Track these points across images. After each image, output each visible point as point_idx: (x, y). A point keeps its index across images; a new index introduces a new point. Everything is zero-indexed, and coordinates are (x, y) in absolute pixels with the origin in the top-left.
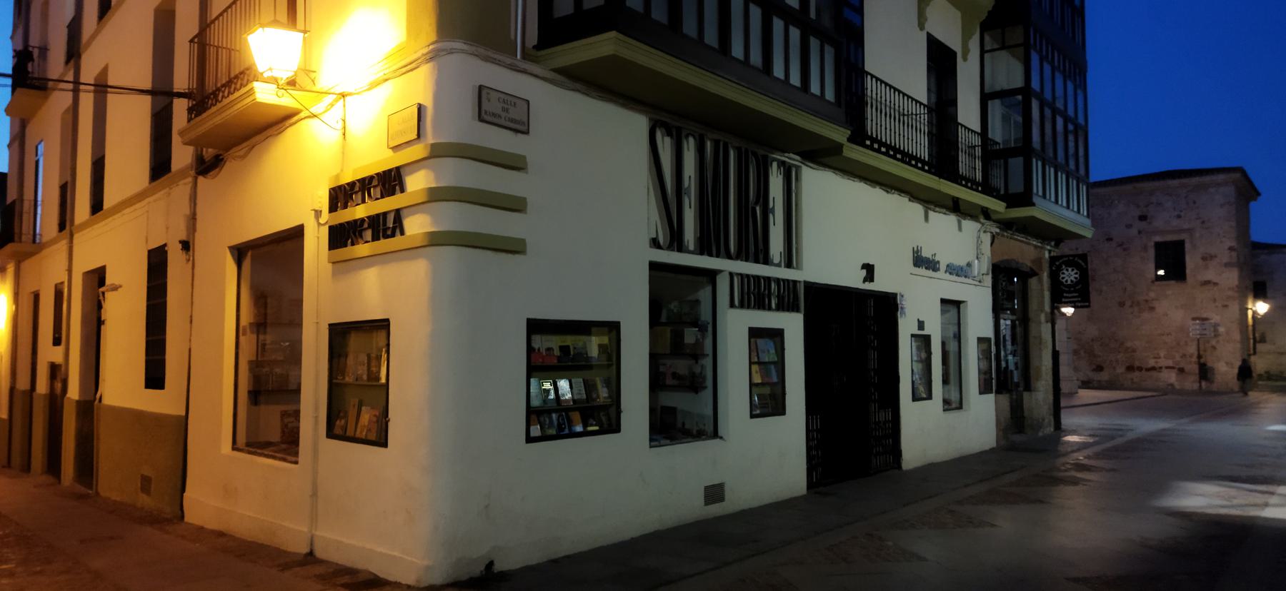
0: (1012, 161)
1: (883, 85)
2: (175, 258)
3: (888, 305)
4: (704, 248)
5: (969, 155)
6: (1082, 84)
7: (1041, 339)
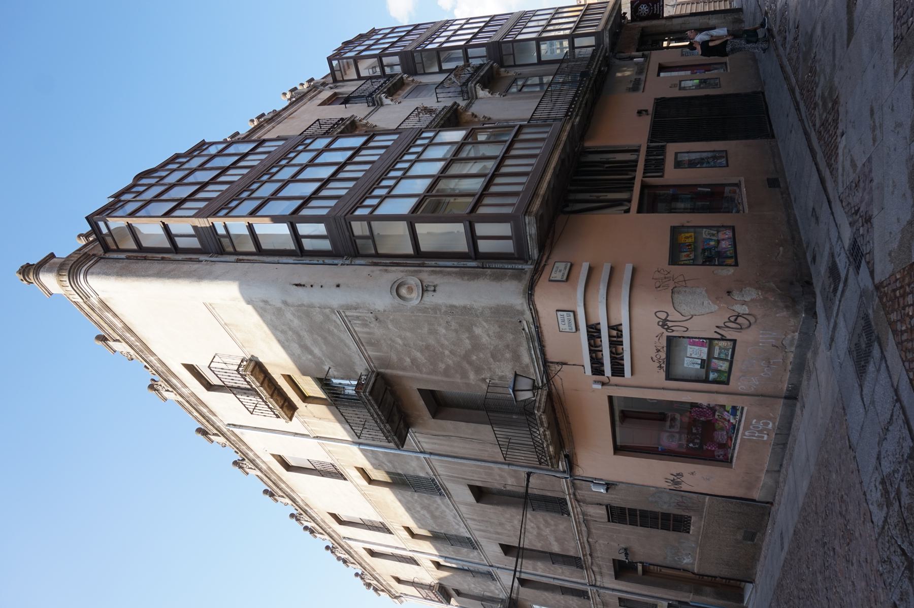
2: (617, 499)
3: (661, 104)
4: (630, 189)
6: (534, 13)
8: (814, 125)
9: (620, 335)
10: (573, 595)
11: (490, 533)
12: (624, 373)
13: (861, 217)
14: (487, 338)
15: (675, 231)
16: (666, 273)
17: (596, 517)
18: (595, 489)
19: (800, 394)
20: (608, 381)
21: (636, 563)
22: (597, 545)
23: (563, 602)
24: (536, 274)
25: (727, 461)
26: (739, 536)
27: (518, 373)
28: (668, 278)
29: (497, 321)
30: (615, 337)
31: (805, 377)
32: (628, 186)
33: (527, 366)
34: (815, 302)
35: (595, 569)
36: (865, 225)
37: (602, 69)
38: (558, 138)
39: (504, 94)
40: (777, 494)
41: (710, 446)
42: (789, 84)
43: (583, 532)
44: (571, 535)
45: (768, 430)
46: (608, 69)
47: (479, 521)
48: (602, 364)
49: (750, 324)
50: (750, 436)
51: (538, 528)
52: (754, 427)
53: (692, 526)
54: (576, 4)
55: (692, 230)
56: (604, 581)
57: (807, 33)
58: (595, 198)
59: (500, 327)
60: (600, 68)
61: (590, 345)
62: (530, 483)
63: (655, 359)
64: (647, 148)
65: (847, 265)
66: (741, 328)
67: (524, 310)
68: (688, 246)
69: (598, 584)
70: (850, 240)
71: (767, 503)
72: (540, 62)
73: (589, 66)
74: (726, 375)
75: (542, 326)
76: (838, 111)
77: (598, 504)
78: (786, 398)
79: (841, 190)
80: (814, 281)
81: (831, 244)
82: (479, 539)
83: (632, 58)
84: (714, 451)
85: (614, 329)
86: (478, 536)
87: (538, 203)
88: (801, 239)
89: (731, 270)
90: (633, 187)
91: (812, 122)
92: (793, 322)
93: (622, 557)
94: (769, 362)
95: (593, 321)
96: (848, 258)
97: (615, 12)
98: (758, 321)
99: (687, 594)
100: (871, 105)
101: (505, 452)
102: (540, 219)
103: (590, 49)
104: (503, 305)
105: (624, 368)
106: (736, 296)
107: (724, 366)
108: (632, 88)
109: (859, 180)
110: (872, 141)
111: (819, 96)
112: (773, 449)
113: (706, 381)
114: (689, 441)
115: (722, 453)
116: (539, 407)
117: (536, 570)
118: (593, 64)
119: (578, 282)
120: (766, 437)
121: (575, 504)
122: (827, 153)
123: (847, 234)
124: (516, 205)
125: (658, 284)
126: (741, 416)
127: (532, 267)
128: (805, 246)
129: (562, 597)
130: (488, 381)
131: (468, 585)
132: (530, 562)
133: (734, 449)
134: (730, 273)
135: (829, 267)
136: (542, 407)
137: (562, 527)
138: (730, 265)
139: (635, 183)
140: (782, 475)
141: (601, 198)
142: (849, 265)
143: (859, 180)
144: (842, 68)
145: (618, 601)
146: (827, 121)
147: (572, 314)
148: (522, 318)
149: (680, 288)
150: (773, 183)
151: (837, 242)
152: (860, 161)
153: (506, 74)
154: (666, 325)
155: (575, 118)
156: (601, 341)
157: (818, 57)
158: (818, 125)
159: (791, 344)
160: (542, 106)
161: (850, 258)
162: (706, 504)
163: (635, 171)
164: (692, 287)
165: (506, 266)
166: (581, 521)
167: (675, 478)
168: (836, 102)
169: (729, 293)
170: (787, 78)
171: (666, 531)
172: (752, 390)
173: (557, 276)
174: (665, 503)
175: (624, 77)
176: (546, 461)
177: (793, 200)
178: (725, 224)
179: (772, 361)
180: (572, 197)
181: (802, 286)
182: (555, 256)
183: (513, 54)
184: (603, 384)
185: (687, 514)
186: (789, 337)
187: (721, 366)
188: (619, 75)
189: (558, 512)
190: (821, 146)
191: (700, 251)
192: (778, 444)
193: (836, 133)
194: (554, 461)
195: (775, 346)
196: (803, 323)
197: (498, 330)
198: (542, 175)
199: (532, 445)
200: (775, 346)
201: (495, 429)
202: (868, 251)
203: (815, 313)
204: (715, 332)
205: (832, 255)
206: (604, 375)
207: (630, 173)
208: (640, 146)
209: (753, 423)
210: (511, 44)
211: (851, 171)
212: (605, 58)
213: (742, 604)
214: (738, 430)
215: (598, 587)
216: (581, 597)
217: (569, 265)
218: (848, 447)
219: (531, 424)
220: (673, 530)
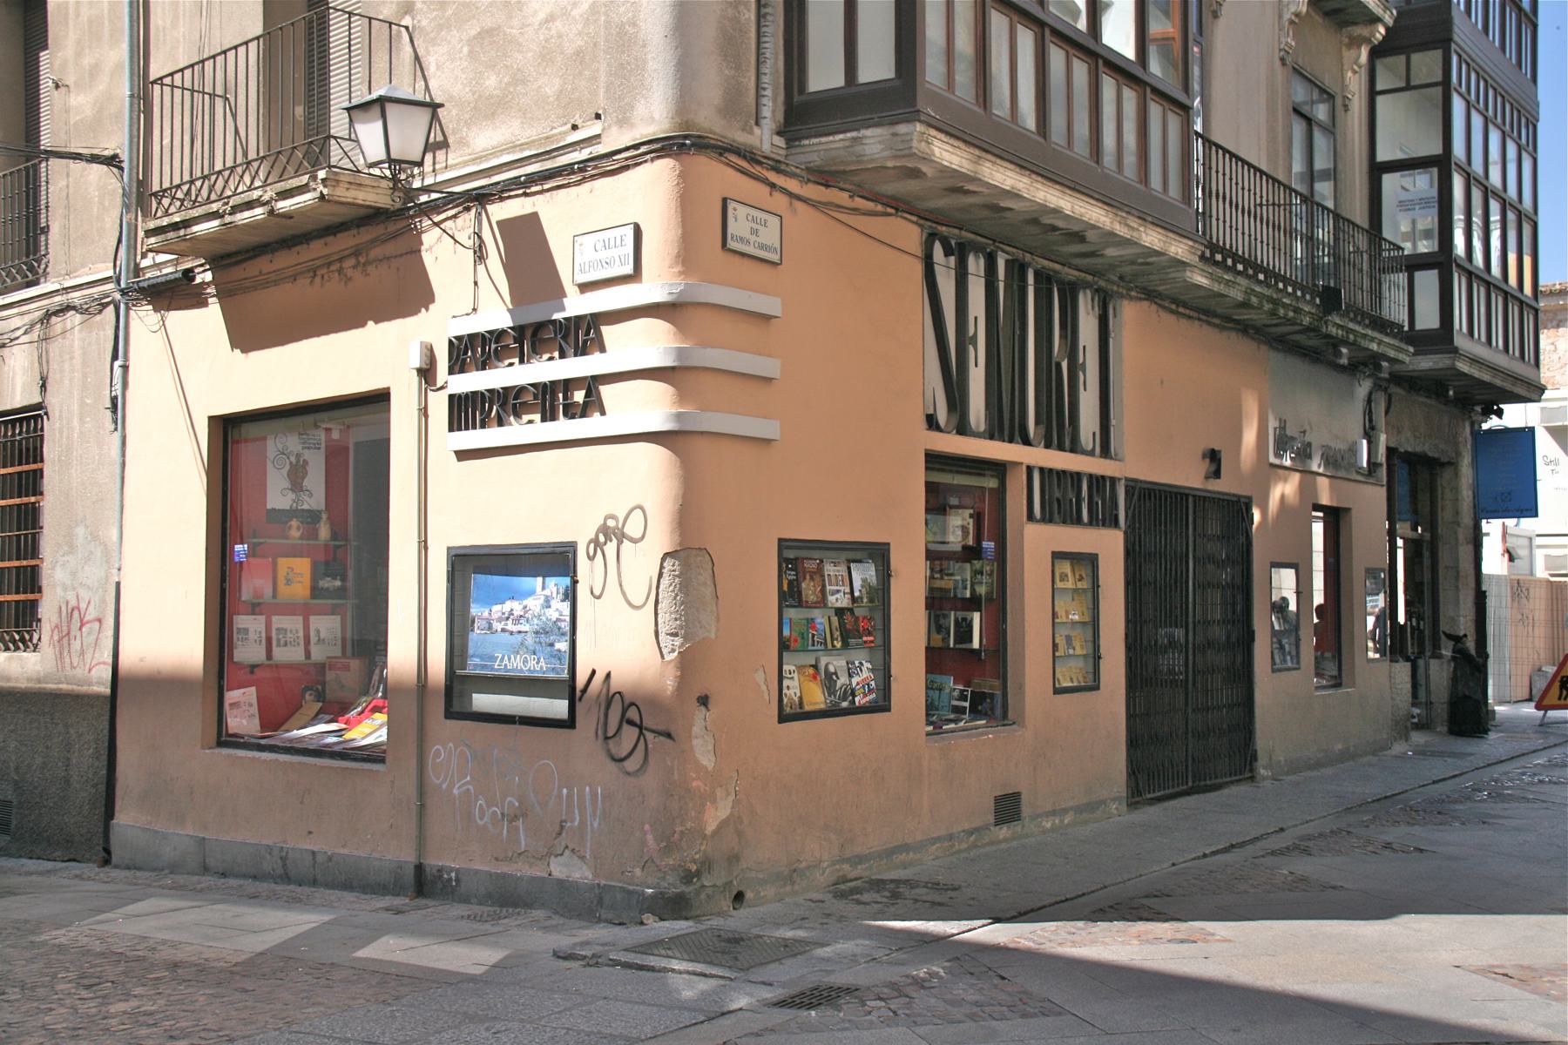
0: (1419, 276)
1: (1220, 152)
6: (1529, 147)
7: (1458, 572)
9: (572, 411)
14: (542, 15)
29: (595, 45)
31: (477, 909)
32: (1006, 425)
37: (1344, 351)
39: (1289, 60)
40: (139, 874)
48: (483, 366)
54: (1542, 282)
60: (1346, 343)
62: (83, 164)
66: (607, 738)
67: (632, 126)
71: (108, 851)
75: (587, 186)
78: (419, 868)
83: (1370, 433)
97: (1508, 386)
101: (178, 81)
103: (1402, 317)
112: (269, 849)
121: (36, 310)
130: (407, 21)
140: (195, 878)
141: (971, 348)
147: (628, 269)
154: (608, 539)
160: (1247, 177)
163: (1048, 446)
172: (434, 779)
174: (74, 574)
176: (166, 213)
180: (976, 265)
185: (45, 638)
197: (569, 49)
199: (212, 165)
201: (253, 46)
206: (451, 372)
207: (1042, 429)
217: (775, 257)
219: (283, 159)
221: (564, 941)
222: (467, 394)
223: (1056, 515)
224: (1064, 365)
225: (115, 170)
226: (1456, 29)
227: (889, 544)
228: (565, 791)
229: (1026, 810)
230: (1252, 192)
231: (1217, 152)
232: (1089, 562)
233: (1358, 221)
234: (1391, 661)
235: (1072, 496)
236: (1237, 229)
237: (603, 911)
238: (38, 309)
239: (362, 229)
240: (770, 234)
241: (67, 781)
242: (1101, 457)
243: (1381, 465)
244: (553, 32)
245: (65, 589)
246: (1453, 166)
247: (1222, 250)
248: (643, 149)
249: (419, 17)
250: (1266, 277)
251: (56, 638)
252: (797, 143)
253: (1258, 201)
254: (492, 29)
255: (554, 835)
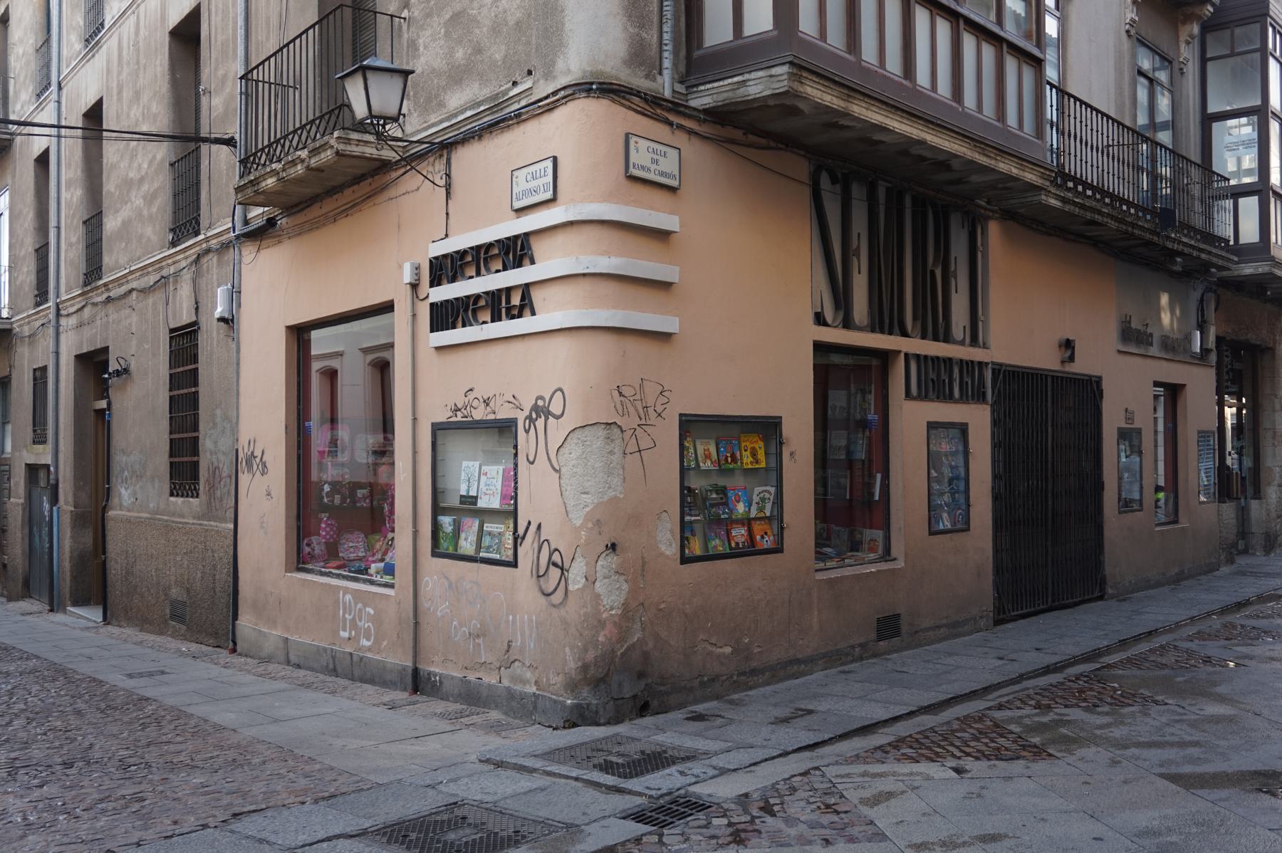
0: (1243, 201)
2: (210, 339)
3: (1090, 389)
4: (879, 324)
5: (1225, 209)
7: (1275, 433)
8: (1000, 707)
10: (38, 272)
11: (119, 73)
12: (437, 331)
13: (752, 821)
15: (769, 428)
16: (659, 409)
17: (174, 303)
18: (221, 293)
19: (424, 698)
20: (421, 297)
21: (108, 397)
22: (128, 311)
23: (23, 253)
24: (646, 100)
25: (300, 560)
26: (174, 592)
27: (410, 77)
28: (646, 414)
30: (508, 301)
32: (884, 321)
33: (441, 105)
34: (598, 724)
35: (87, 310)
36: (730, 830)
38: (1002, 152)
39: (1133, 32)
40: (249, 660)
41: (328, 525)
42: (1108, 650)
43: (146, 278)
44: (138, 254)
45: (357, 639)
46: (1178, 273)
47: (136, 44)
48: (453, 279)
49: (549, 595)
50: (344, 603)
51: (142, 180)
52: (360, 610)
53: (182, 499)
55: (773, 465)
56: (70, 333)
57: (1215, 684)
58: (855, 245)
59: (517, 23)
60: (1181, 254)
61: (489, 246)
63: (471, 396)
64: (980, 363)
65: (653, 793)
66: (539, 576)
68: (733, 456)
69: (63, 321)
70: (710, 795)
71: (235, 643)
72: (1208, 120)
73: (1188, 227)
74: (451, 550)
76: (1018, 758)
77: (197, 303)
78: (416, 671)
79: (831, 772)
80: (648, 720)
81: (716, 754)
82: (104, 47)
83: (1202, 326)
84: (319, 535)
85: (523, 299)
86: (110, 45)
87: (828, 98)
88: (751, 688)
89: (669, 546)
90: (882, 332)
91: (1008, 702)
92: (557, 680)
93: (113, 366)
94: (478, 636)
95: (538, 247)
96: (670, 793)
98: (554, 610)
99: (71, 499)
100: (1006, 836)
102: (784, 105)
103: (1229, 233)
104: (563, 24)
105: (447, 329)
106: (607, 563)
107: (467, 545)
108: (1130, 327)
109: (838, 813)
110: (920, 841)
111: (1064, 715)
112: (325, 650)
113: (437, 510)
114: (334, 485)
115: (317, 551)
116: (348, 141)
117: (68, 187)
118: (1191, 238)
119: (627, 204)
120: (345, 634)
122: (927, 737)
123: (723, 790)
124: (980, 116)
125: (625, 391)
126: (380, 585)
127: (667, 94)
128: (736, 696)
129: (31, 249)
130: (405, 14)
131: (21, 41)
132: (79, 172)
133: (322, 574)
134: (663, 548)
135: (665, 752)
136: (349, 148)
137: (149, 231)
138: (682, 547)
139: (892, 337)
140: (281, 667)
141: (855, 259)
142: (651, 797)
143: (838, 813)
144: (1114, 763)
145: (40, 366)
146: (1002, 736)
147: (549, 195)
148: (537, 74)
149: (618, 442)
150: (889, 627)
151: (715, 768)
152: (882, 816)
153: (1183, 37)
154: (539, 416)
155: (1058, 197)
156: (498, 271)
157: (1154, 709)
158: (998, 715)
159: (515, 679)
161: (667, 798)
162: (223, 525)
163: (924, 337)
164: (623, 468)
165: (667, 28)
166: (165, 273)
167: (258, 460)
168: (1039, 752)
169: (613, 547)
170: (1123, 644)
171: (168, 448)
172: (425, 604)
173: (642, 155)
174: (216, 443)
175: (1158, 310)
177: (846, 668)
178: (786, 533)
179: (480, 641)
180: (858, 192)
181: (635, 697)
182: (696, 152)
183: (1232, 54)
184: (414, 286)
185: (201, 488)
186: (528, 675)
187: (466, 539)
188: (1164, 299)
189: (175, 219)
190: (948, 723)
191: (722, 482)
192: (334, 658)
193: (968, 755)
194: (249, 191)
195: (509, 646)
196: (555, 702)
198: (903, 111)
200: (509, 646)
202: (665, 839)
203: (574, 725)
204: (529, 523)
205: (691, 757)
206: (431, 286)
208: (985, 346)
209: (367, 609)
210: (1258, 46)
211: (867, 794)
212: (1207, 266)
213: (69, 603)
214: (356, 580)
215: (58, 321)
216: (38, 289)
217: (675, 183)
218: (237, 810)
220: (171, 463)
221: (494, 744)
222: (442, 303)
223: (931, 393)
224: (938, 273)
225: (232, 149)
226: (1271, 6)
227: (781, 417)
228: (511, 617)
229: (904, 628)
230: (1100, 133)
231: (1069, 99)
232: (963, 429)
233: (1193, 159)
234: (1219, 502)
235: (945, 377)
236: (1086, 162)
237: (537, 715)
238: (193, 254)
239: (376, 177)
240: (669, 163)
241: (214, 589)
242: (971, 346)
243: (1211, 350)
244: (500, 9)
245: (211, 454)
246: (1270, 114)
247: (1074, 179)
248: (562, 93)
249: (412, 10)
250: (1112, 201)
251: (207, 489)
252: (695, 89)
253: (1105, 143)
254: (460, 13)
255: (504, 652)
